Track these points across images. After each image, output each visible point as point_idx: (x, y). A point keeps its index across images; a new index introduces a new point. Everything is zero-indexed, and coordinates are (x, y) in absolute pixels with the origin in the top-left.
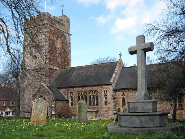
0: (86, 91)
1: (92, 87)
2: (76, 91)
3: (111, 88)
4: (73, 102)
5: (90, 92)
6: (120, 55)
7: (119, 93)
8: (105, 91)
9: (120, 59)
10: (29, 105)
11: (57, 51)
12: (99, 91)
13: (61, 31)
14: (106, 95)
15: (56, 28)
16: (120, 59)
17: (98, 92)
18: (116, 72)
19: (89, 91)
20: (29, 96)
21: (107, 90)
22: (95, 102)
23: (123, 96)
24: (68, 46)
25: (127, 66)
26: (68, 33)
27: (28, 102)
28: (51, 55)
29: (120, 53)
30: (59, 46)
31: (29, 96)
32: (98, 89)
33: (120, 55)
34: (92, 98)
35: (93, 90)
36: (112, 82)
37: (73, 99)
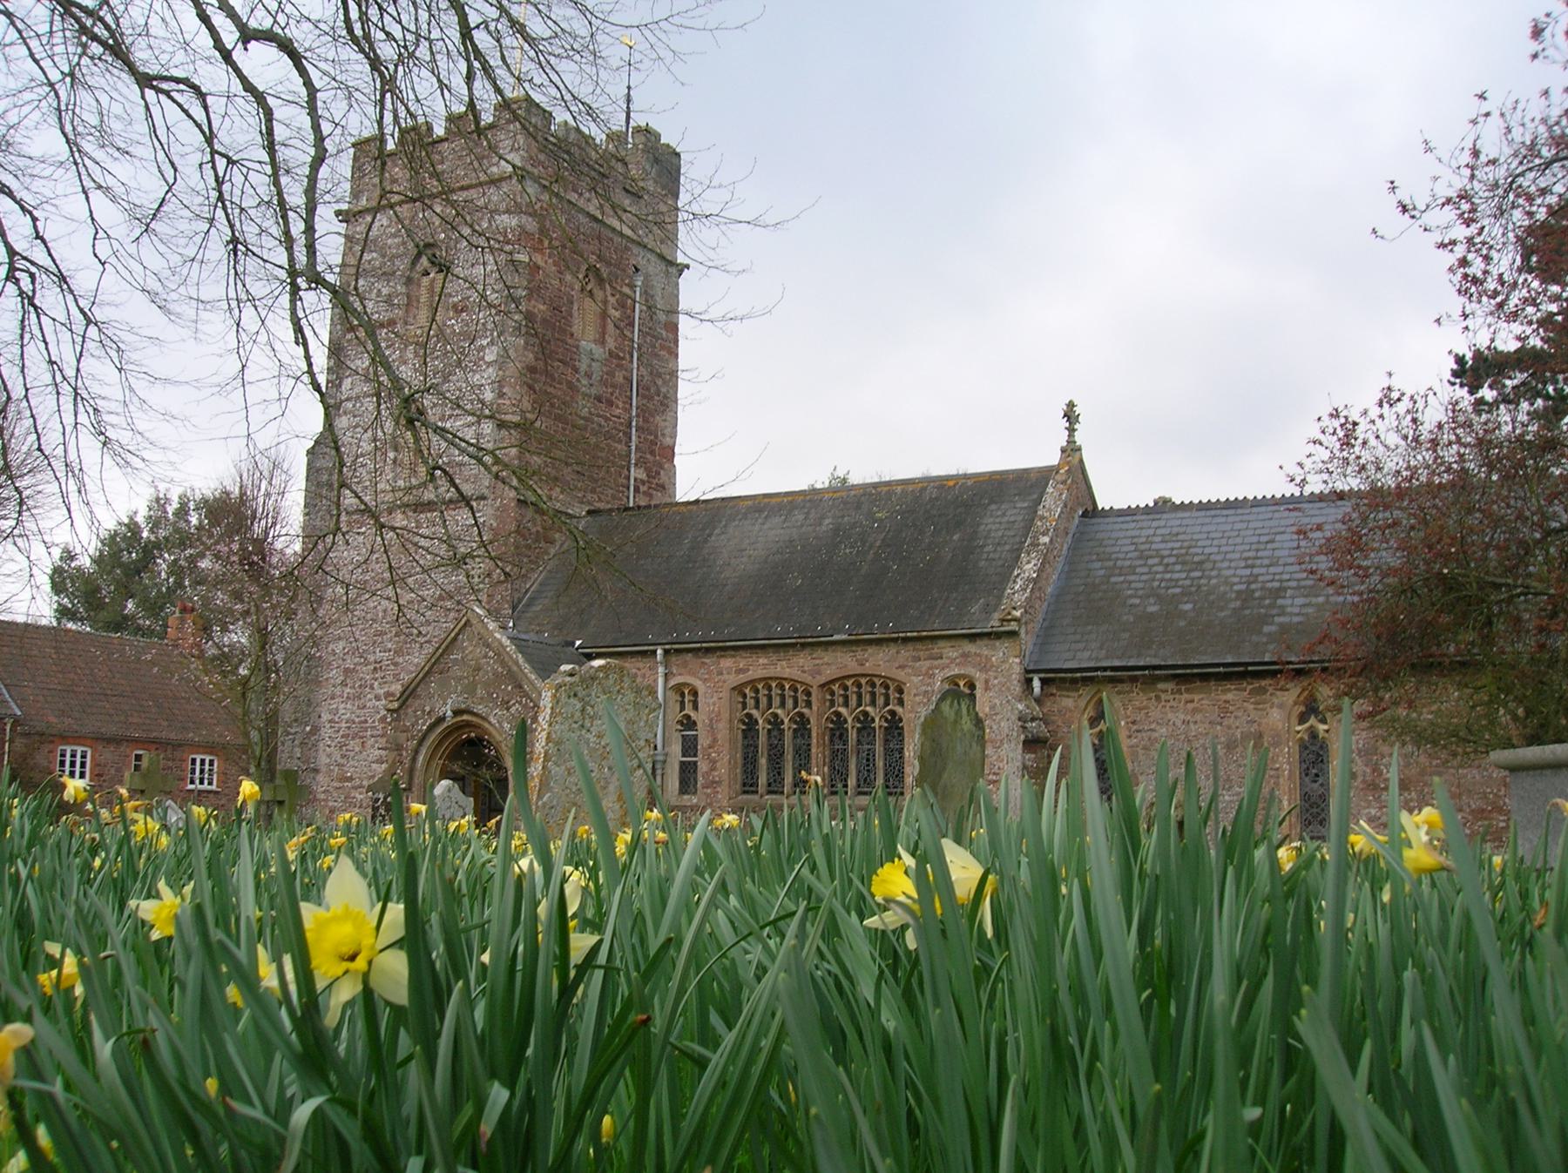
0: (808, 679)
1: (860, 654)
2: (734, 680)
3: (1007, 662)
4: (703, 767)
5: (835, 687)
6: (1071, 415)
7: (1068, 702)
8: (683, 695)
9: (1071, 450)
10: (351, 779)
11: (584, 382)
12: (915, 679)
13: (618, 239)
14: (688, 717)
15: (581, 210)
16: (1071, 450)
17: (901, 692)
18: (1046, 539)
19: (833, 681)
20: (346, 710)
21: (698, 683)
22: (880, 764)
23: (1312, 721)
24: (663, 347)
25: (1120, 504)
26: (666, 252)
27: (337, 756)
28: (538, 406)
29: (1071, 405)
30: (589, 344)
31: (346, 710)
32: (902, 667)
33: (1071, 415)
34: (852, 736)
35: (859, 670)
36: (1017, 614)
37: (703, 742)
